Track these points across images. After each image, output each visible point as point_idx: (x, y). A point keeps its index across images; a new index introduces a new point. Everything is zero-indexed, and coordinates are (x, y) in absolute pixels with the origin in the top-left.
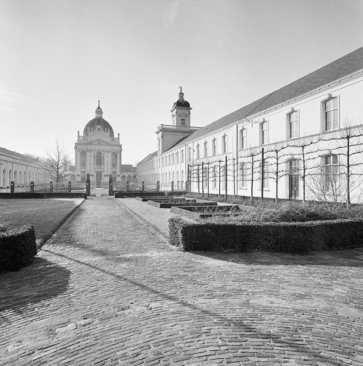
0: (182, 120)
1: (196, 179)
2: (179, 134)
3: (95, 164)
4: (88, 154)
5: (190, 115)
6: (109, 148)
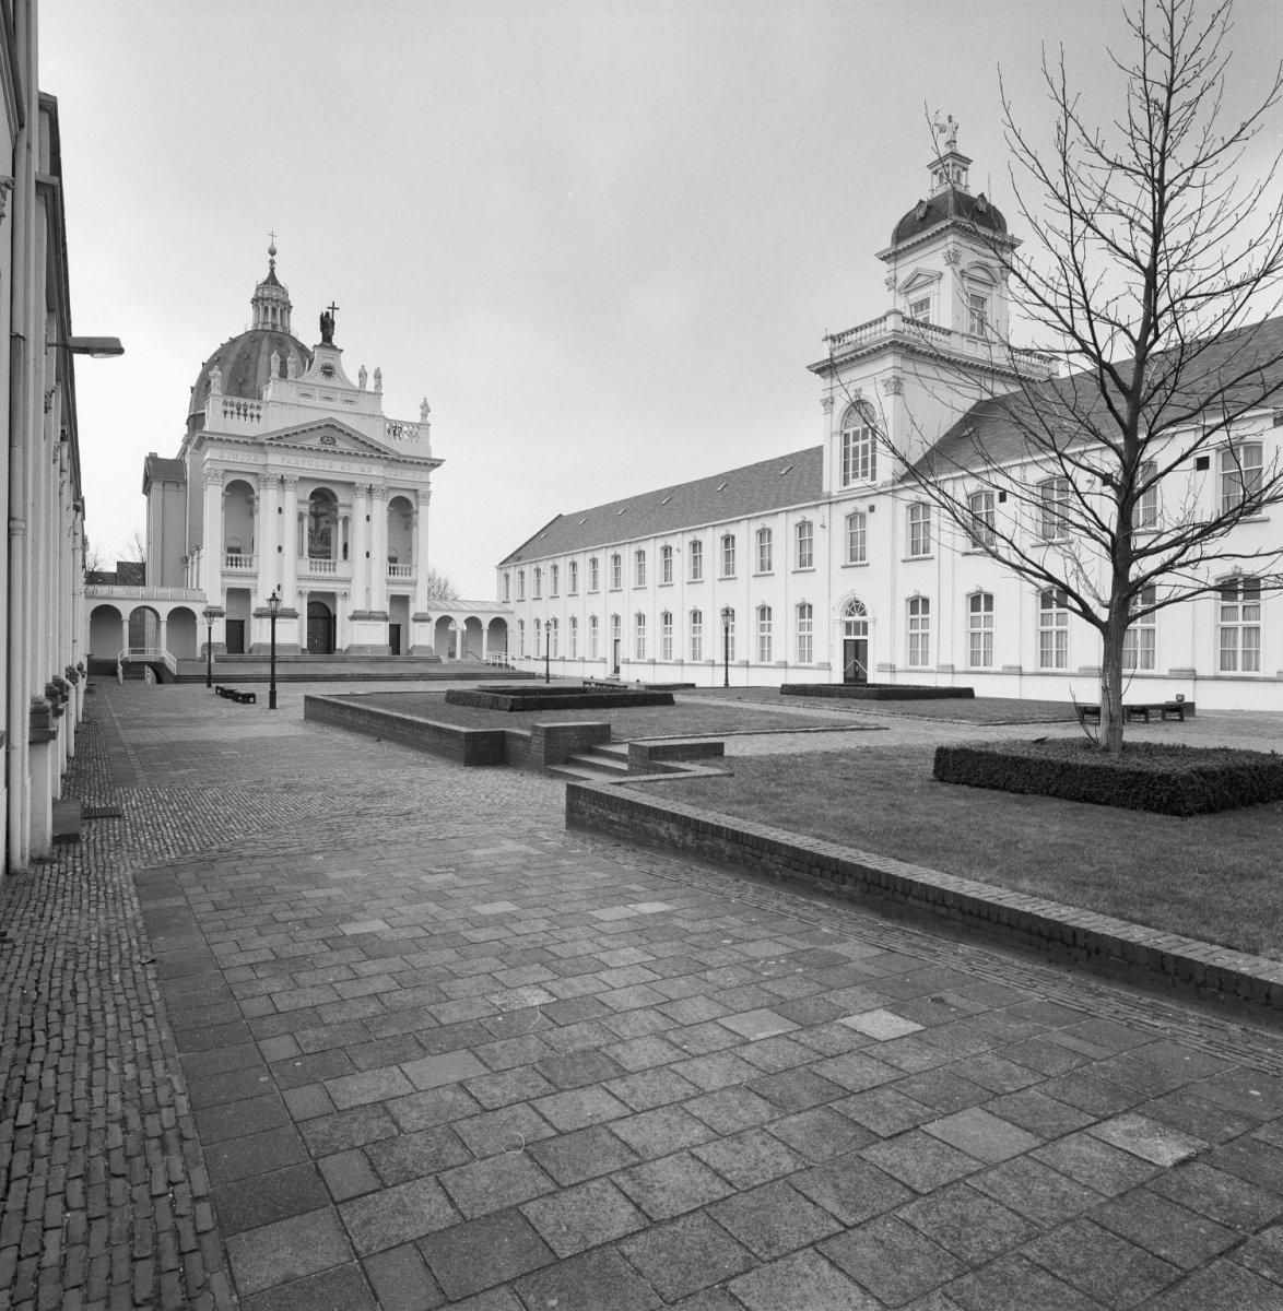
3: (301, 554)
4: (267, 499)
6: (376, 472)
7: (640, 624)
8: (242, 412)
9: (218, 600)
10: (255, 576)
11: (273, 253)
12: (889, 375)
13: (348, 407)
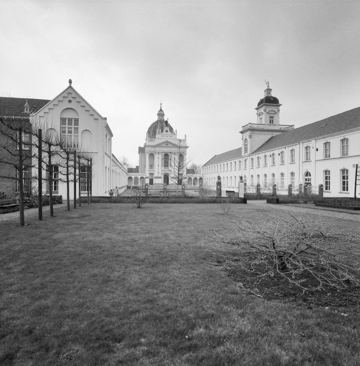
0: (270, 117)
1: (64, 178)
2: (267, 133)
4: (156, 156)
5: (279, 112)
7: (282, 177)
8: (152, 141)
9: (148, 175)
10: (154, 171)
11: (161, 104)
12: (249, 135)
13: (171, 138)
